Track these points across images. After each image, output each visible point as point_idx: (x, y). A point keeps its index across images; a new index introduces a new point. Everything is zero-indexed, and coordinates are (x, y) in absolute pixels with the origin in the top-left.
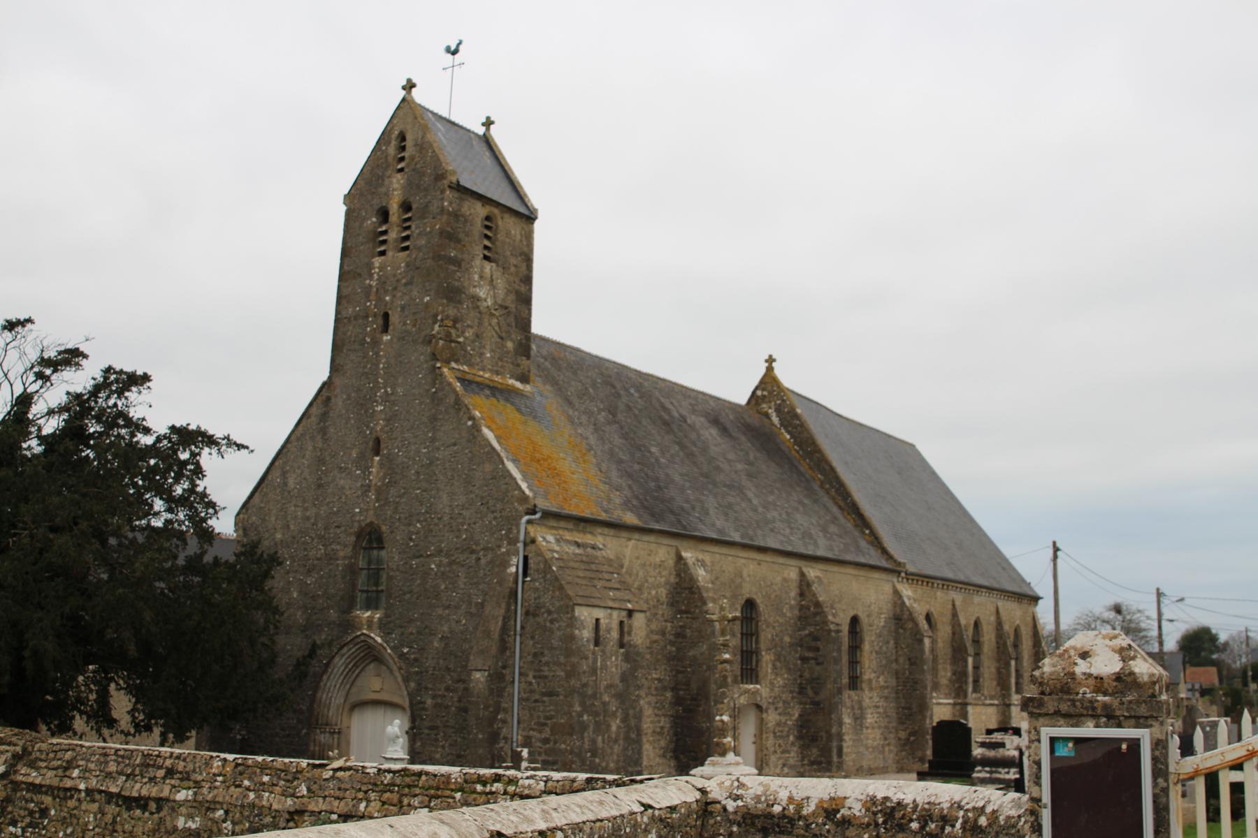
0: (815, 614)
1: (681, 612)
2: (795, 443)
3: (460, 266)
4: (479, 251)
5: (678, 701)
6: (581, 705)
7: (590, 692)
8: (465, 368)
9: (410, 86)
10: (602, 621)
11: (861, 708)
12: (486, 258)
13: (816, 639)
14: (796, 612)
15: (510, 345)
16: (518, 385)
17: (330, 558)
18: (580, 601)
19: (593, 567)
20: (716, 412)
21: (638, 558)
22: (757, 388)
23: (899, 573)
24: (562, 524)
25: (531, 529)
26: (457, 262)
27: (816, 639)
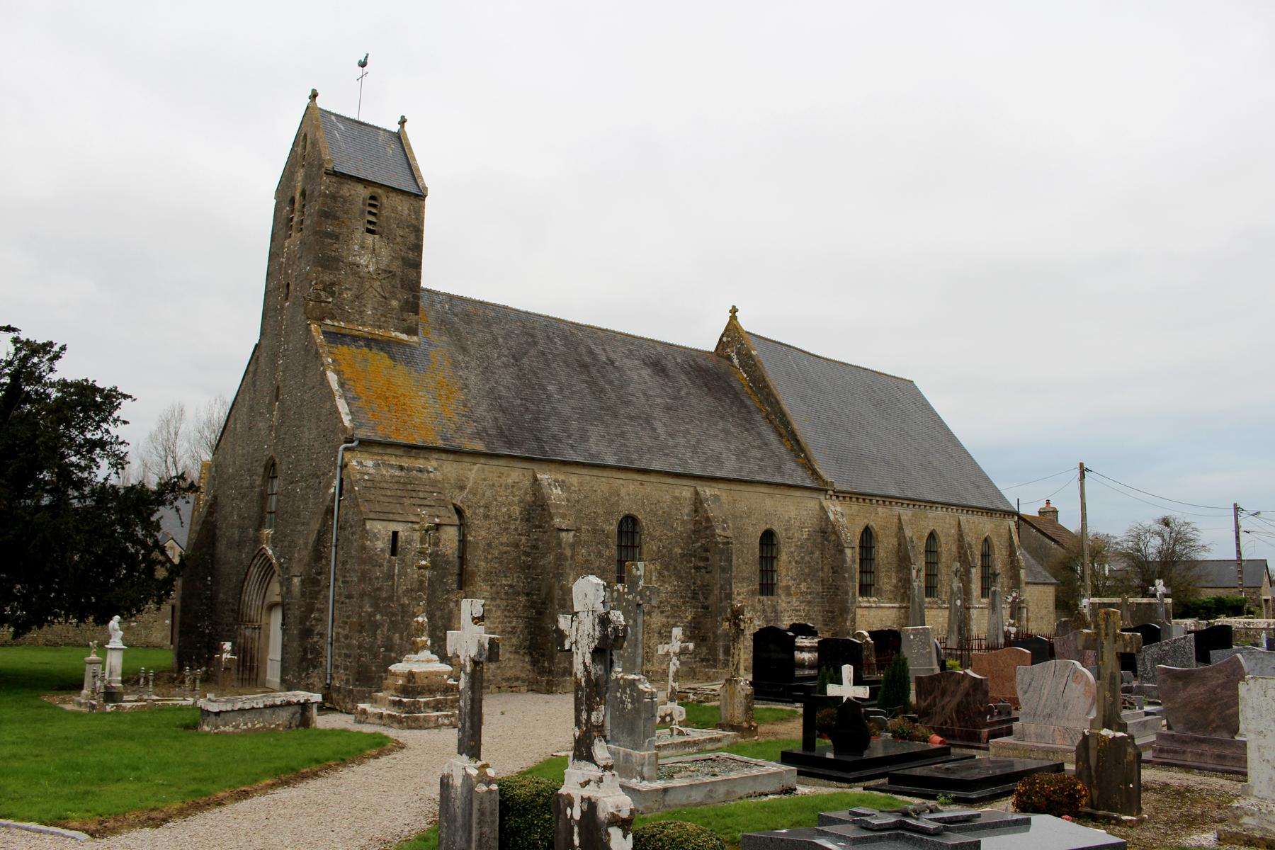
0: (707, 528)
1: (536, 527)
2: (751, 381)
3: (337, 238)
4: (360, 227)
5: (533, 605)
6: (371, 606)
7: (384, 595)
8: (342, 324)
9: (314, 95)
10: (401, 534)
11: (776, 612)
12: (369, 231)
13: (706, 550)
14: (691, 526)
15: (395, 303)
16: (404, 337)
17: (252, 486)
18: (371, 516)
19: (409, 487)
20: (661, 359)
21: (485, 480)
22: (723, 335)
23: (826, 491)
24: (389, 451)
25: (348, 455)
26: (335, 236)
27: (706, 550)
